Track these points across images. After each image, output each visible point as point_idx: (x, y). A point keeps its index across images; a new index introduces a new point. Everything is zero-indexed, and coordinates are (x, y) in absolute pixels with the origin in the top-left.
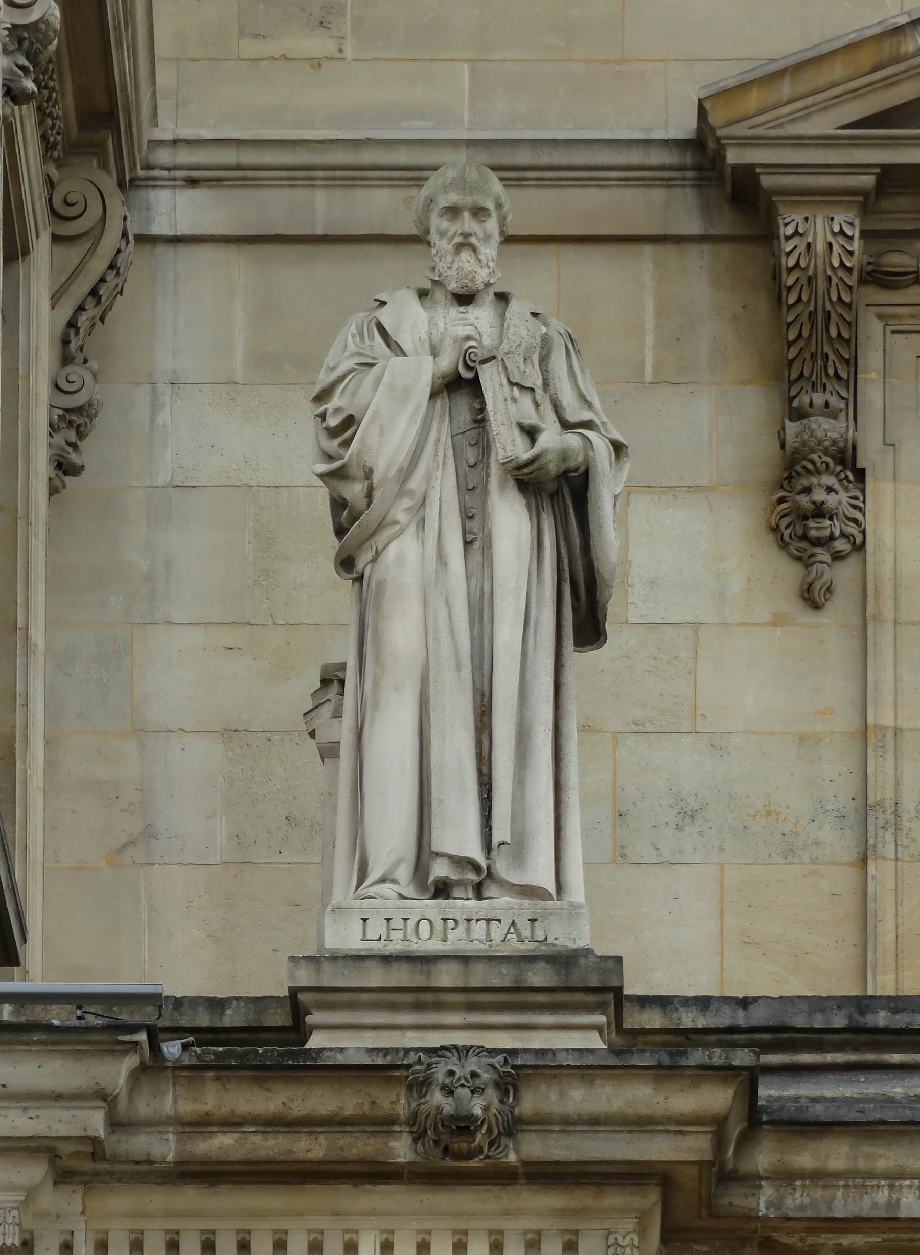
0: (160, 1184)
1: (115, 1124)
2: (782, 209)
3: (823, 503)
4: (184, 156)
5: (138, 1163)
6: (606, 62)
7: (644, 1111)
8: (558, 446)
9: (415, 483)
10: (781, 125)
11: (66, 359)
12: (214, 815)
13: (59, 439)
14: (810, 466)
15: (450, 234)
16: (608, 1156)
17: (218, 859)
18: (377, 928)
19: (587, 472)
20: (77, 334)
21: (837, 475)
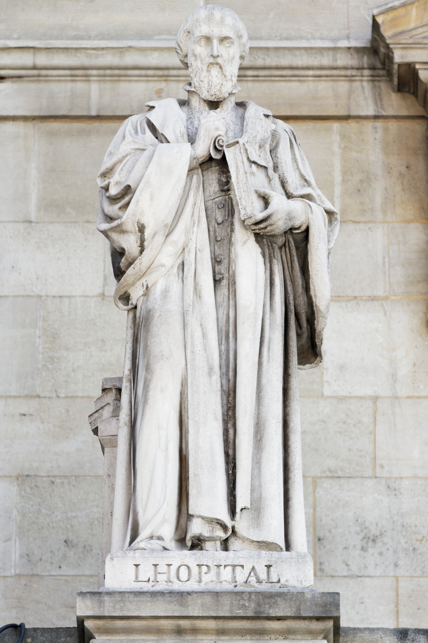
12: (9, 539)
17: (13, 572)
18: (146, 572)
19: (307, 230)
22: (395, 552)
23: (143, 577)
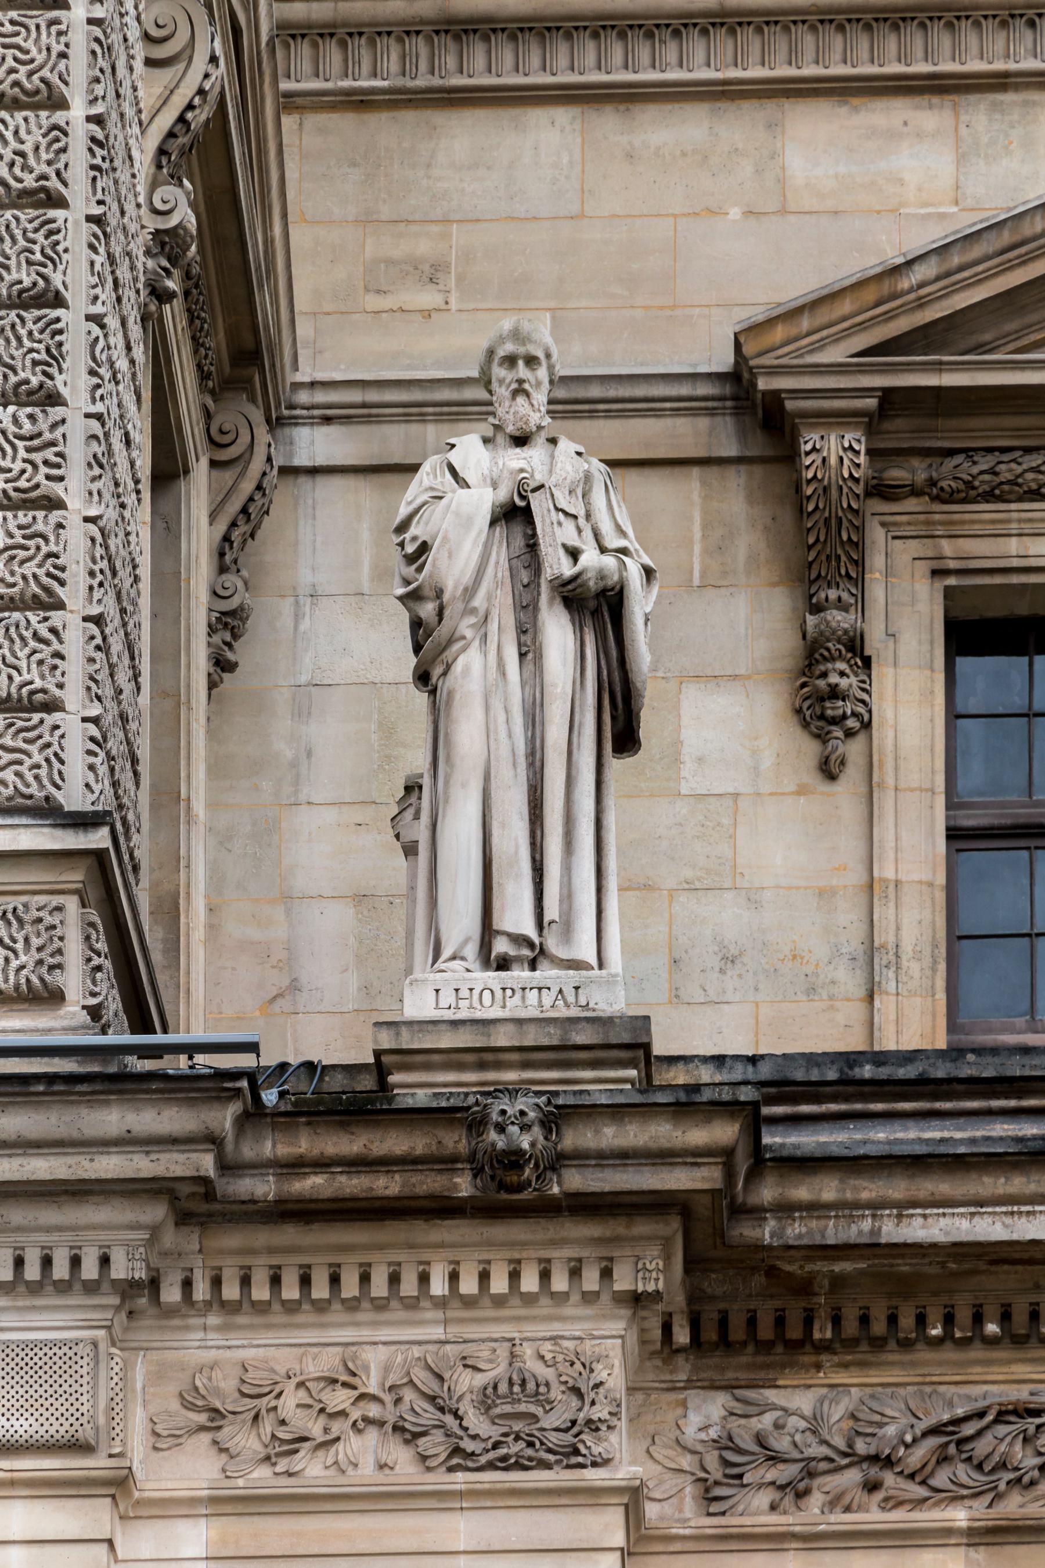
0: (264, 1223)
1: (224, 1166)
2: (801, 427)
3: (837, 685)
4: (321, 397)
5: (243, 1202)
6: (662, 308)
7: (665, 1144)
8: (596, 565)
9: (479, 601)
10: (801, 356)
11: (222, 569)
13: (217, 639)
14: (826, 653)
15: (507, 381)
16: (635, 1187)
18: (448, 997)
20: (231, 548)
21: (848, 662)
22: (755, 974)
23: (443, 1004)
